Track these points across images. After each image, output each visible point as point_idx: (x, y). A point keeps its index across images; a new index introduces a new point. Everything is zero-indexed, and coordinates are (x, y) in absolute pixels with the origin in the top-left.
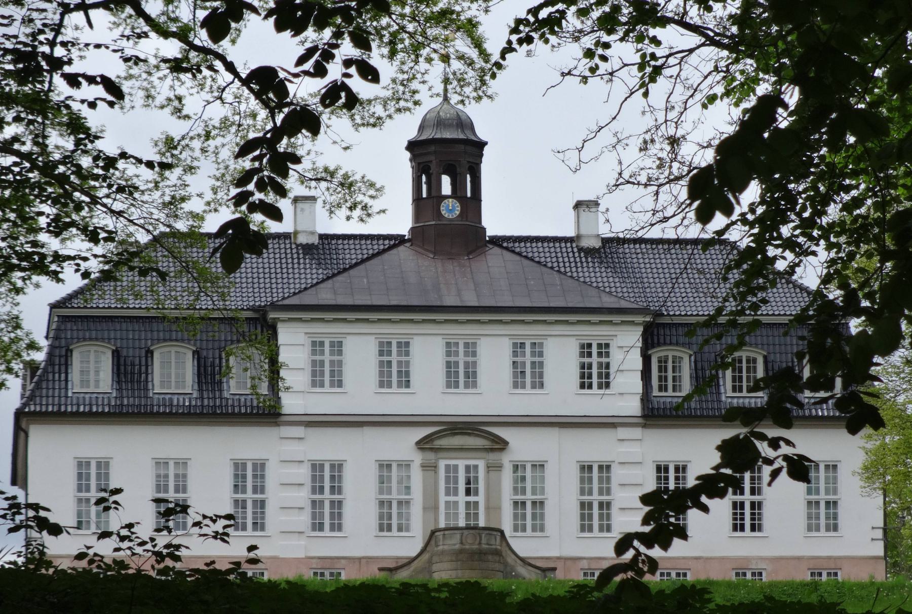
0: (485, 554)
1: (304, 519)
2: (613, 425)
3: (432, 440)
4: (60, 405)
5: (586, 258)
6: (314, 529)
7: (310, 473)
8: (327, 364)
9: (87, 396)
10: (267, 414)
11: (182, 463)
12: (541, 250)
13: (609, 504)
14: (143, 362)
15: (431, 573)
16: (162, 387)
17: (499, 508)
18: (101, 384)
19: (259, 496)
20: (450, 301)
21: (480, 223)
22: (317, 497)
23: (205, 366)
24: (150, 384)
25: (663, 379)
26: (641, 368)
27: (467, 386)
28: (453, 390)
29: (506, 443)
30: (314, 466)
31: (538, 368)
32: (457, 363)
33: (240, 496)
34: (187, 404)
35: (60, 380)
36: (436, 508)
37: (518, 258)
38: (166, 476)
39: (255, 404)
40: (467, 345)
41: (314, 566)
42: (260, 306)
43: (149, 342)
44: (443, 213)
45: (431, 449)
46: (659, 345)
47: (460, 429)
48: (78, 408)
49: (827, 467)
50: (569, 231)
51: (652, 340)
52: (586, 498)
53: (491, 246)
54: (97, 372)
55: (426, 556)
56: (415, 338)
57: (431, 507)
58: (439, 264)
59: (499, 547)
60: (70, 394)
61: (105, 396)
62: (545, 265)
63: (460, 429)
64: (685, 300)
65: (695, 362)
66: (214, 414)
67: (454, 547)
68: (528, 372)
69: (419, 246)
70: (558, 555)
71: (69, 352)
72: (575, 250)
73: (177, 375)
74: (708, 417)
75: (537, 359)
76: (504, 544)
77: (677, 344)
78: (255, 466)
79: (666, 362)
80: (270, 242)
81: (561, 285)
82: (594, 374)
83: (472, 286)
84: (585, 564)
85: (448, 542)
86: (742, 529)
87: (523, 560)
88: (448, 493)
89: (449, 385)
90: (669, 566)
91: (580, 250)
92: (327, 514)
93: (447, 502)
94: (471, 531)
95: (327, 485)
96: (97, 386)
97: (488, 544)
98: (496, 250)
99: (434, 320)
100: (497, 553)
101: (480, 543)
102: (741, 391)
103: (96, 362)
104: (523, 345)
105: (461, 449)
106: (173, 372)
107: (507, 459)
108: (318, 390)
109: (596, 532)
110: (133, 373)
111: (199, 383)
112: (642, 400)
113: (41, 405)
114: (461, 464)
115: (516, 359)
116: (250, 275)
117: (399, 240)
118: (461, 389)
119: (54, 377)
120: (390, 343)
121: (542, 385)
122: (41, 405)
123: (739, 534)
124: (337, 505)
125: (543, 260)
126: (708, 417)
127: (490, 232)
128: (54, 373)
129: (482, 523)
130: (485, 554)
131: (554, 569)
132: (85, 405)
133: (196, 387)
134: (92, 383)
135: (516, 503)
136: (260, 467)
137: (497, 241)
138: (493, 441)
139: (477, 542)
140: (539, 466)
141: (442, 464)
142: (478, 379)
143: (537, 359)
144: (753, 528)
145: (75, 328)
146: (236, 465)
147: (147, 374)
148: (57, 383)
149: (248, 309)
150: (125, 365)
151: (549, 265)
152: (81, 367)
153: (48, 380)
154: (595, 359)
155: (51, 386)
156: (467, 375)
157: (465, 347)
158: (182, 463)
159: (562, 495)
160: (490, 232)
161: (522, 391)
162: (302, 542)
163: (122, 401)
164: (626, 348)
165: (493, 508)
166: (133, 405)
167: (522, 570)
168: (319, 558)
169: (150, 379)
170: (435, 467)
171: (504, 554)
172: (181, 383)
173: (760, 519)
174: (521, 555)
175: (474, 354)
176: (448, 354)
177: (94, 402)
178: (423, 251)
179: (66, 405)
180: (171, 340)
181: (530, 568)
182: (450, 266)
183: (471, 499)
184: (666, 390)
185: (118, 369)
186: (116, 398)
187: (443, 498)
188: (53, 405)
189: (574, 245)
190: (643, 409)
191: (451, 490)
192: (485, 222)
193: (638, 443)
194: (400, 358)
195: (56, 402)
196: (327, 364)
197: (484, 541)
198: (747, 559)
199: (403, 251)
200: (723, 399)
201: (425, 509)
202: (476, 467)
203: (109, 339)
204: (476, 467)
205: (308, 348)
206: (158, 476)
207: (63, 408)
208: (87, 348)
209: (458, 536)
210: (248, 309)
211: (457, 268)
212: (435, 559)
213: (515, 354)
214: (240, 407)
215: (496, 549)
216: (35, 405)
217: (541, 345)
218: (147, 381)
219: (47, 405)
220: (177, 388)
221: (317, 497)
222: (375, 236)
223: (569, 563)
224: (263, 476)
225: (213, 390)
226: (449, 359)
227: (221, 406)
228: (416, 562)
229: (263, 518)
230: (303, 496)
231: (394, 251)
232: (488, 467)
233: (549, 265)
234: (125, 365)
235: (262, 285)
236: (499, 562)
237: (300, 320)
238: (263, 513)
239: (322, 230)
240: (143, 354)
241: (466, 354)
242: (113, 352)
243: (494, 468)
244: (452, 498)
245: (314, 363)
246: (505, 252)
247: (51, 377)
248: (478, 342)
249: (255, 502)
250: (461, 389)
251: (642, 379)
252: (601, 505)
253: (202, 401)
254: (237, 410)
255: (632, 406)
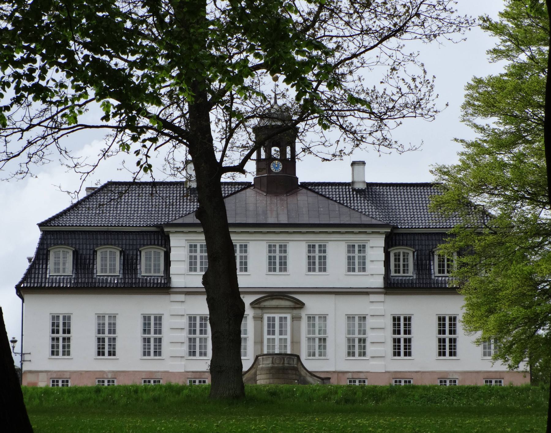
0: (287, 369)
1: (184, 349)
2: (367, 293)
3: (260, 303)
4: (42, 283)
5: (357, 195)
6: (190, 355)
7: (188, 322)
8: (198, 258)
9: (58, 278)
10: (163, 287)
11: (113, 317)
12: (388, 190)
13: (364, 341)
14: (92, 258)
15: (256, 381)
16: (146, 272)
17: (299, 343)
18: (66, 270)
19: (158, 336)
20: (271, 220)
21: (295, 175)
22: (192, 336)
23: (128, 260)
24: (95, 270)
25: (397, 266)
26: (384, 259)
27: (281, 270)
28: (272, 273)
29: (303, 304)
30: (190, 318)
31: (323, 260)
32: (275, 257)
33: (147, 336)
34: (116, 282)
35: (42, 268)
36: (262, 342)
37: (316, 195)
38: (104, 324)
39: (156, 282)
40: (281, 246)
41: (190, 377)
42: (161, 224)
43: (138, 246)
44: (272, 169)
45: (259, 308)
46: (396, 245)
47: (276, 295)
48: (52, 284)
49: (110, 317)
50: (348, 179)
51: (392, 243)
52: (101, 336)
53: (301, 188)
54: (64, 264)
55: (253, 371)
56: (251, 242)
57: (259, 342)
58: (269, 199)
59: (296, 366)
60: (48, 276)
61: (69, 277)
62: (332, 200)
63: (276, 295)
64: (412, 219)
65: (417, 255)
66: (131, 288)
67: (268, 366)
68: (317, 262)
69: (258, 189)
70: (334, 370)
71: (48, 252)
72: (351, 190)
73: (110, 265)
74: (423, 288)
75: (322, 254)
76: (299, 364)
77: (407, 245)
78: (156, 318)
79: (399, 255)
80: (222, 187)
81: (339, 211)
82: (356, 264)
83: (286, 211)
84: (350, 376)
85: (265, 362)
86: (444, 354)
87: (310, 373)
88: (269, 333)
89: (270, 270)
90: (400, 376)
91: (354, 190)
92: (152, 346)
93: (268, 339)
94: (278, 356)
95: (198, 329)
96: (64, 272)
97: (288, 364)
98: (304, 191)
99: (301, 232)
100: (295, 369)
101: (283, 363)
102: (443, 273)
103: (64, 258)
104: (314, 246)
105: (277, 308)
106: (108, 263)
107: (304, 314)
108: (193, 273)
109: (448, 356)
110: (85, 264)
111: (123, 269)
112: (384, 278)
113: (31, 283)
114: (277, 316)
115: (310, 255)
116: (418, 208)
117: (247, 185)
118: (278, 272)
119: (39, 266)
120: (354, 245)
121: (325, 270)
122: (31, 283)
123: (442, 358)
124: (408, 341)
125: (331, 196)
126: (423, 288)
127: (300, 181)
128: (39, 264)
129: (289, 352)
130: (287, 369)
131: (329, 378)
132: (56, 283)
133: (122, 272)
134: (61, 270)
135: (309, 339)
136: (159, 319)
137: (305, 185)
138: (295, 303)
139: (282, 362)
140: (324, 318)
141: (266, 316)
142: (287, 266)
143: (322, 254)
144: (451, 354)
145: (52, 238)
146: (145, 318)
147: (93, 264)
148: (41, 270)
149: (153, 226)
150: (81, 259)
151: (335, 199)
152: (55, 261)
153: (35, 269)
154: (356, 254)
155: (37, 272)
156: (281, 264)
157: (280, 248)
158: (113, 317)
159: (337, 336)
160: (300, 181)
161: (314, 273)
162: (183, 362)
163: (78, 280)
164: (375, 248)
165: (295, 342)
166: (85, 283)
167: (309, 379)
168: (193, 372)
169: (95, 267)
170: (261, 318)
171: (299, 370)
172: (113, 270)
173: (455, 349)
174: (310, 370)
175: (285, 251)
176: (270, 251)
177: (62, 281)
178: (261, 192)
179: (45, 283)
180: (108, 244)
181: (315, 378)
182: (275, 200)
183: (283, 337)
184: (399, 272)
185: (77, 262)
186: (74, 278)
187: (266, 337)
188: (38, 283)
189: (350, 187)
190: (385, 284)
191: (271, 332)
192: (298, 175)
193: (382, 303)
194: (242, 254)
195: (40, 281)
196: (198, 258)
197: (286, 362)
198: (447, 373)
199: (250, 192)
200: (433, 277)
201: (255, 343)
202: (286, 318)
203: (72, 244)
204: (286, 318)
205: (187, 249)
206: (99, 324)
207: (43, 285)
208: (58, 250)
209: (271, 359)
210: (153, 226)
211: (279, 201)
212: (258, 372)
213: (309, 251)
214: (147, 283)
215: (294, 367)
216: (27, 283)
217: (325, 246)
218: (93, 268)
219: (34, 283)
220: (110, 272)
221: (192, 336)
222: (148, 183)
223: (340, 375)
224: (160, 324)
225: (132, 274)
226: (270, 254)
227: (135, 283)
228: (247, 374)
229: (160, 349)
230: (184, 336)
231: (244, 192)
232: (293, 318)
233: (335, 199)
234: (81, 259)
235: (164, 212)
236: (295, 374)
237: (182, 232)
238: (160, 346)
239: (368, 180)
240: (92, 253)
241: (281, 251)
242: (74, 252)
243: (296, 319)
244: (271, 337)
245: (191, 257)
246: (309, 192)
247: (37, 267)
248: (287, 244)
249: (155, 339)
250: (278, 272)
251: (385, 266)
252: (360, 340)
253: (125, 280)
254: (43, 285)
255: (379, 282)
